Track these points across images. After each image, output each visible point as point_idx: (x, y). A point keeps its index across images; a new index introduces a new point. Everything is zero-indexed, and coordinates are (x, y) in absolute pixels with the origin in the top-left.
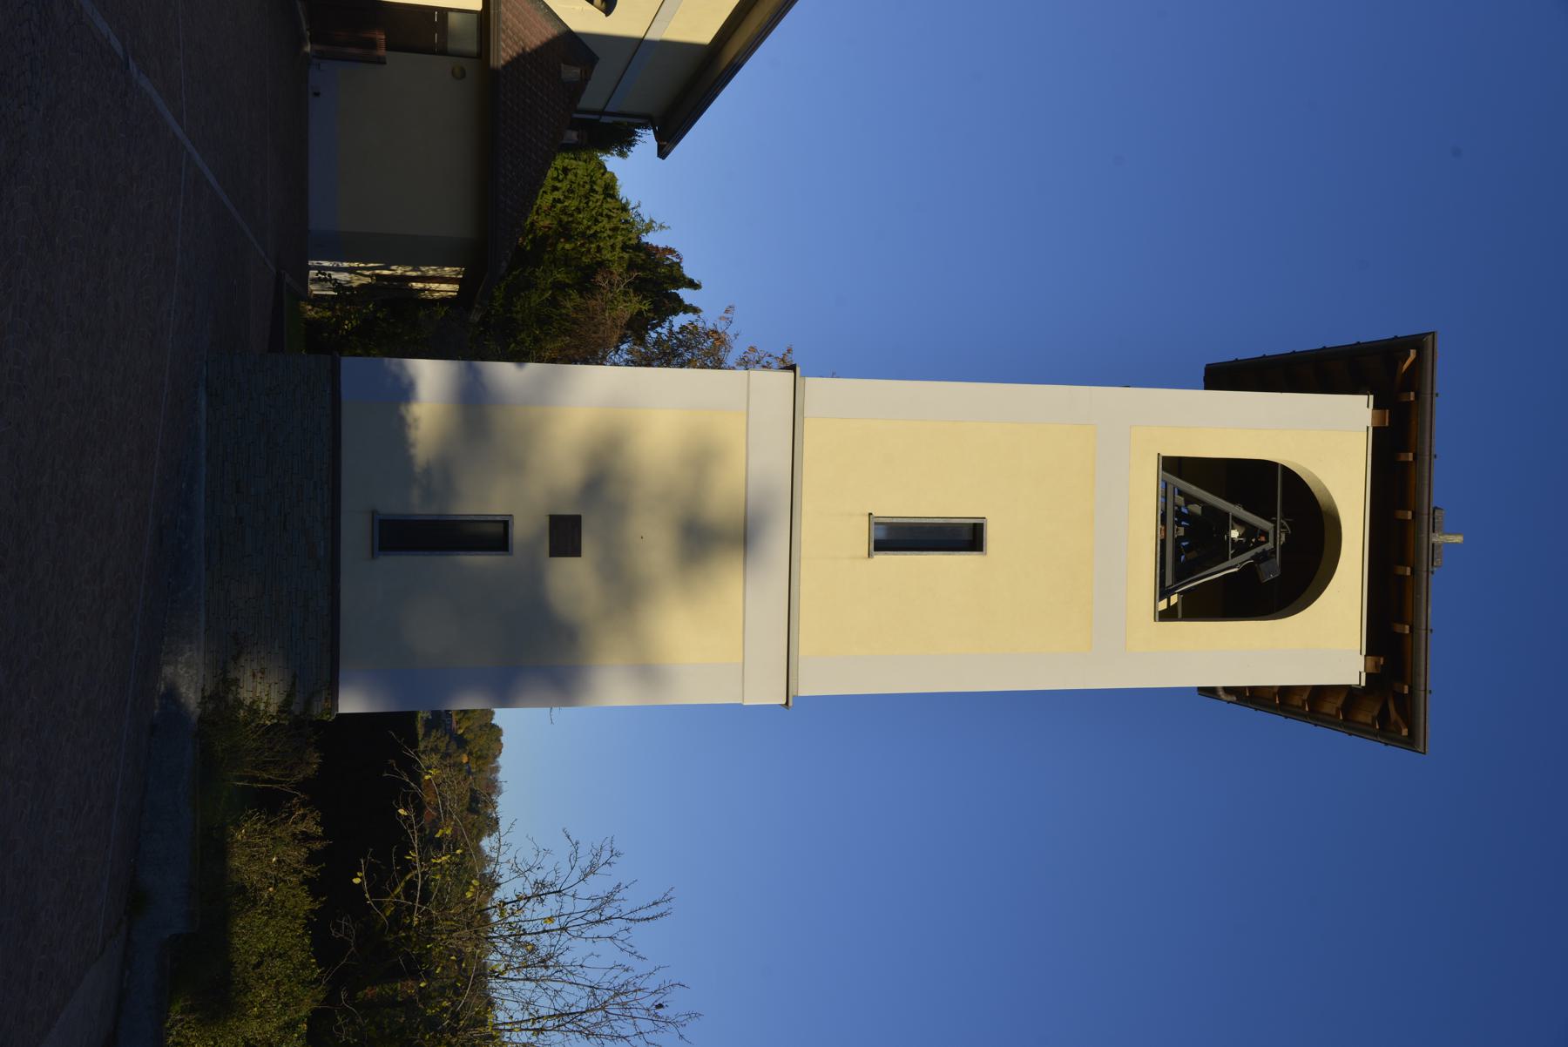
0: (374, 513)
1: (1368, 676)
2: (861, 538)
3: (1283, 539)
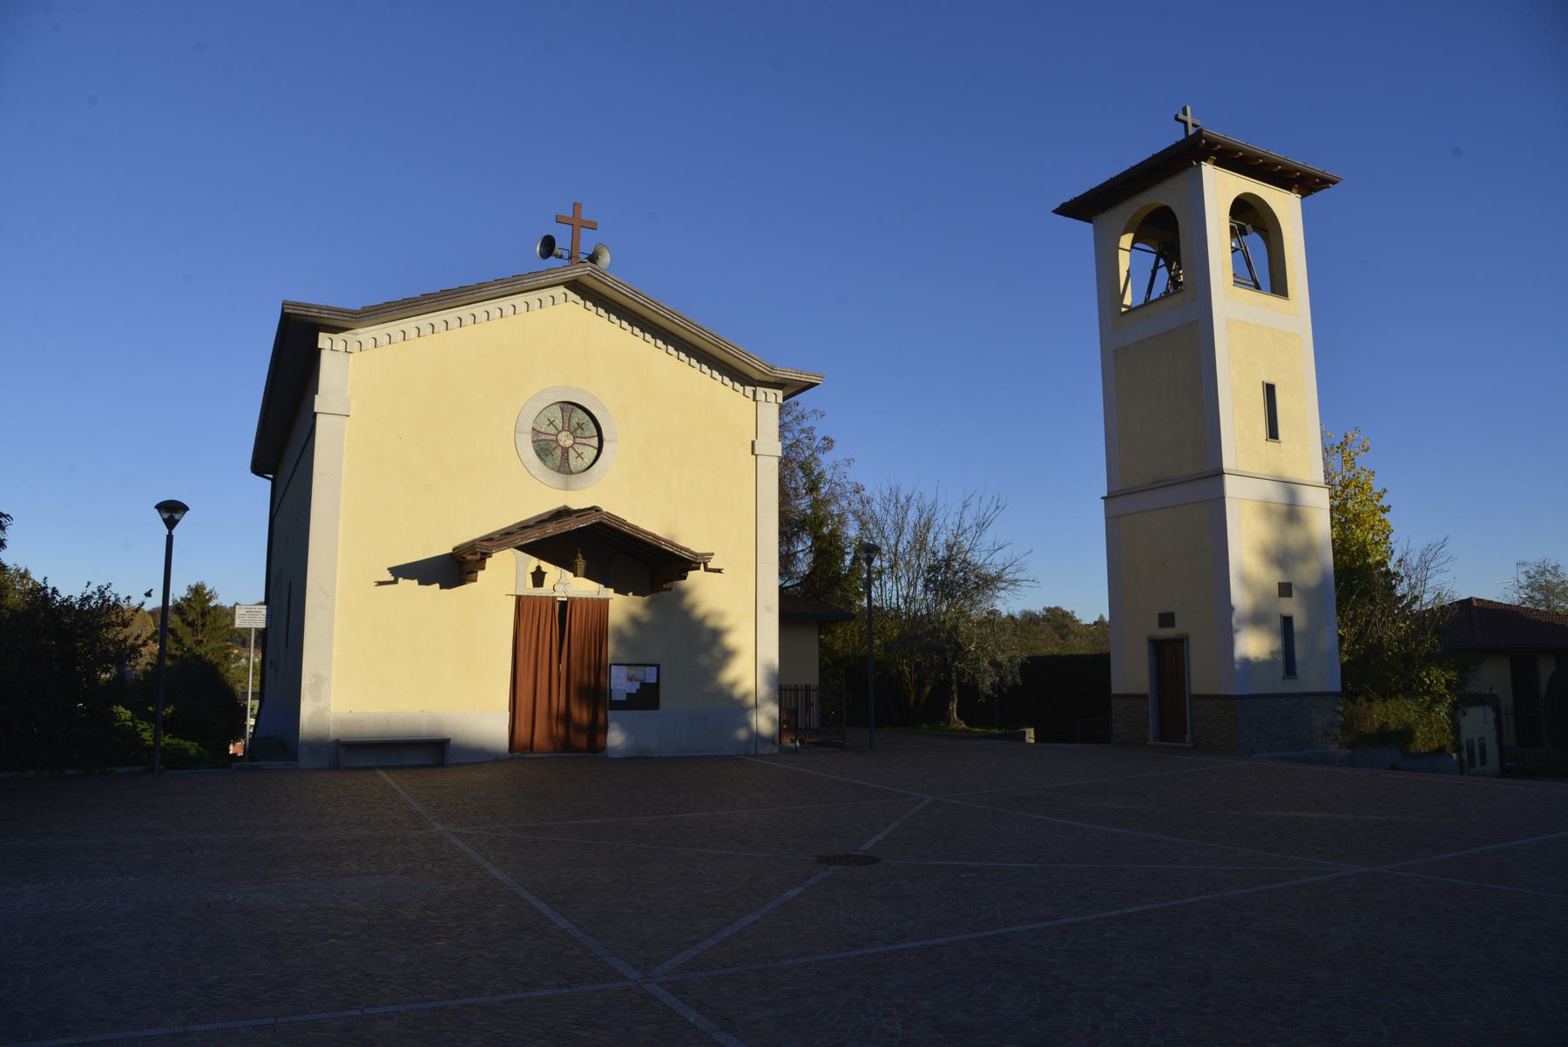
0: (1284, 678)
1: (1298, 193)
2: (1272, 444)
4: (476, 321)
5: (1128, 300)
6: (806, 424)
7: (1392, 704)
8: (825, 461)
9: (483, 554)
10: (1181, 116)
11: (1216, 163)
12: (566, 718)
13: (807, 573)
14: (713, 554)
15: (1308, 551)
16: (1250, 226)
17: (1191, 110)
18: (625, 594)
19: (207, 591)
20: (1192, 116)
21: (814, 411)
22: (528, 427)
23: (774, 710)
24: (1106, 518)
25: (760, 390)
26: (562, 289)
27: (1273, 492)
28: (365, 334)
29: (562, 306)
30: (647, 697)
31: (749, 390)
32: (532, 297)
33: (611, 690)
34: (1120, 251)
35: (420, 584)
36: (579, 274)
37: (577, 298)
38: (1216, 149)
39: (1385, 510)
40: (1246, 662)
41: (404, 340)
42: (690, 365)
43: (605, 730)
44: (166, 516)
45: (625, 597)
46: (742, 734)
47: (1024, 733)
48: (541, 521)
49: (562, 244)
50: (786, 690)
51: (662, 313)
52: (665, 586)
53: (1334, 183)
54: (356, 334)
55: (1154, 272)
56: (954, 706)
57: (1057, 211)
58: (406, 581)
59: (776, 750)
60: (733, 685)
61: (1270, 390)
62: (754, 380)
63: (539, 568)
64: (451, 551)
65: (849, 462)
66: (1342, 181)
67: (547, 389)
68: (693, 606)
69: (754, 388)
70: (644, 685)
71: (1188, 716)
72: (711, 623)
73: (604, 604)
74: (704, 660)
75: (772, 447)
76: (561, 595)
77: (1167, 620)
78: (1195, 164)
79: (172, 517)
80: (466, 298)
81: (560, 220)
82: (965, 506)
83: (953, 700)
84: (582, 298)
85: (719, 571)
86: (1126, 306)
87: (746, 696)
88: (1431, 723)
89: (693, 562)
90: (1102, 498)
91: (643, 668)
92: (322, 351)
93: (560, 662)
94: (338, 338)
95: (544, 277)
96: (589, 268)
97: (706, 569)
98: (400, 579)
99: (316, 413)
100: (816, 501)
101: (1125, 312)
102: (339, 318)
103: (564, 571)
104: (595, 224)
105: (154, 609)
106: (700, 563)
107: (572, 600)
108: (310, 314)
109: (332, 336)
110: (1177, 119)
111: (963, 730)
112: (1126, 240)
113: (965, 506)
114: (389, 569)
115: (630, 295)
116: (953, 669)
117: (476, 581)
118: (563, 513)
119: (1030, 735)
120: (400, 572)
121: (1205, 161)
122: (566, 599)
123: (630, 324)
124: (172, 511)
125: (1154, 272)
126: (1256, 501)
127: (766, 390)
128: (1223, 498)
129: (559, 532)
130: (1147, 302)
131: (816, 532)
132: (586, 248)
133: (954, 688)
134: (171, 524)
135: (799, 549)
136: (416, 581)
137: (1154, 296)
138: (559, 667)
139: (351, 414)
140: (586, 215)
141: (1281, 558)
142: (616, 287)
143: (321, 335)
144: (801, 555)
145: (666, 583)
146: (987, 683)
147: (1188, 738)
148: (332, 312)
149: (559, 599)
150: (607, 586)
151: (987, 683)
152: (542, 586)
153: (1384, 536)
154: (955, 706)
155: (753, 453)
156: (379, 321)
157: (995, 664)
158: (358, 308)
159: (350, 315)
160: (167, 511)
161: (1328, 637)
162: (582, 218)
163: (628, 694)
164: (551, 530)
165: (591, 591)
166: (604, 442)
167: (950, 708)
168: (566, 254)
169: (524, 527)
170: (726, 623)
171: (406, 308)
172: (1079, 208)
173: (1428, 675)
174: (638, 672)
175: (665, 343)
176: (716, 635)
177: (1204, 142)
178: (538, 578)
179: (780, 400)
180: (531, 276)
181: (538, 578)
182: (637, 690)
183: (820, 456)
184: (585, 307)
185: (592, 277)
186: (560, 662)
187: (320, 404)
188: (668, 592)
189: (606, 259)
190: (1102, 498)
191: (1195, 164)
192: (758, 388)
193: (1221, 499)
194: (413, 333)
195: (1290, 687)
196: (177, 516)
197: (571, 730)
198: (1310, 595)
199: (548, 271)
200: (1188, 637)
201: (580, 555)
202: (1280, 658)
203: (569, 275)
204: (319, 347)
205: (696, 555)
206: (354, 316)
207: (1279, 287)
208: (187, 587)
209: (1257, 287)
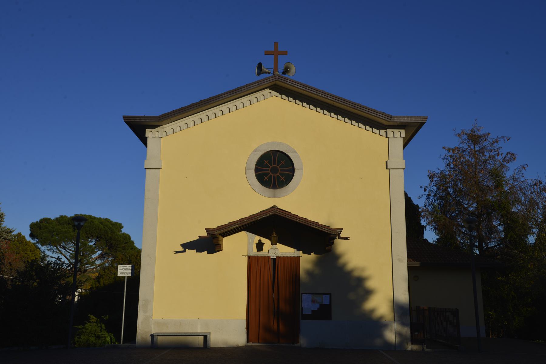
21: (503, 137)
25: (390, 132)
26: (268, 91)
28: (168, 127)
31: (383, 132)
37: (277, 94)
40: (117, 268)
54: (163, 128)
62: (385, 125)
63: (260, 241)
65: (523, 167)
69: (386, 130)
70: (322, 306)
73: (297, 259)
76: (273, 255)
81: (267, 53)
85: (347, 238)
89: (332, 234)
96: (278, 77)
98: (187, 250)
107: (279, 258)
109: (152, 130)
114: (181, 245)
120: (187, 246)
122: (275, 257)
132: (281, 66)
136: (195, 251)
140: (280, 49)
149: (271, 257)
152: (262, 250)
155: (387, 168)
178: (260, 246)
181: (260, 246)
189: (293, 70)
201: (274, 233)
204: (146, 136)
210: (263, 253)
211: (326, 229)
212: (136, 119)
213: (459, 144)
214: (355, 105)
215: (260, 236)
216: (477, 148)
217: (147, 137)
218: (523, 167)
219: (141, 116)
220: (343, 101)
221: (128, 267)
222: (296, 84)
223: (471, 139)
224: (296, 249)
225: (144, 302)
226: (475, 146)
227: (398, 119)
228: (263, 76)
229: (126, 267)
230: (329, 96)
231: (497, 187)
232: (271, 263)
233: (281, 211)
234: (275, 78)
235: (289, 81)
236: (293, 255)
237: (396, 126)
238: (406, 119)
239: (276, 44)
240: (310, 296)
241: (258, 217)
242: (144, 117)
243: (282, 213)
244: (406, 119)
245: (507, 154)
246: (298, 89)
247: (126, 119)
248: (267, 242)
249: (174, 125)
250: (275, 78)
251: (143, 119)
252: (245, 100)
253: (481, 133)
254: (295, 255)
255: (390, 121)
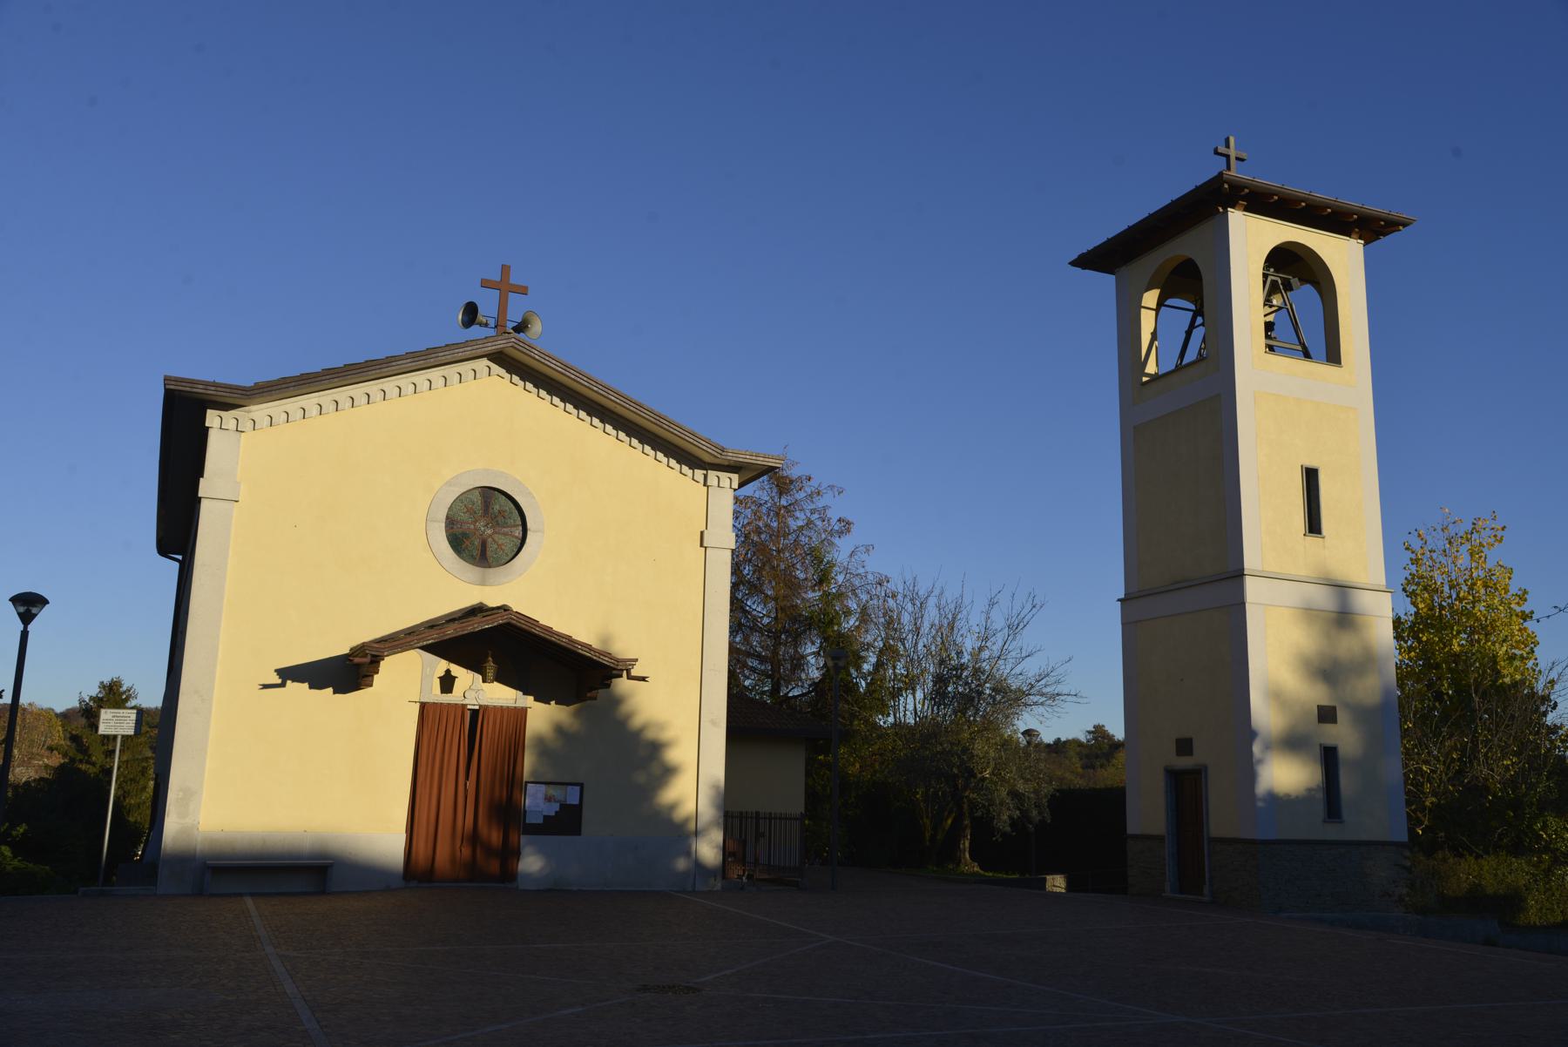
0: (1325, 821)
2: (1312, 540)
3: (1272, 270)
4: (478, 376)
5: (1151, 368)
6: (820, 503)
7: (1489, 863)
8: (841, 552)
9: (373, 656)
10: (1222, 149)
11: (1247, 209)
12: (474, 838)
13: (817, 681)
14: (637, 660)
15: (1367, 661)
16: (1297, 279)
17: (1235, 141)
18: (548, 702)
19: (124, 688)
20: (1236, 148)
21: (831, 487)
22: (442, 515)
23: (717, 836)
24: (1123, 624)
25: (712, 474)
26: (485, 362)
27: (1322, 598)
28: (260, 411)
29: (484, 380)
30: (566, 821)
31: (699, 474)
32: (451, 371)
33: (525, 811)
34: (1143, 310)
35: (311, 688)
36: (501, 346)
37: (502, 372)
38: (1243, 193)
39: (1526, 617)
40: (1273, 798)
41: (304, 418)
42: (630, 445)
43: (517, 854)
44: (22, 609)
45: (547, 705)
46: (681, 864)
47: (1045, 880)
48: (452, 619)
49: (487, 310)
50: (775, 818)
51: (595, 389)
52: (589, 695)
53: (1405, 225)
54: (249, 412)
55: (1189, 334)
56: (966, 844)
57: (1074, 263)
58: (296, 684)
59: (718, 885)
60: (673, 807)
61: (1311, 476)
62: (705, 462)
63: (448, 671)
64: (348, 652)
65: (868, 549)
66: (1415, 223)
67: (465, 472)
68: (629, 716)
69: (705, 472)
70: (565, 807)
71: (1206, 863)
72: (650, 735)
73: (521, 714)
74: (641, 778)
75: (724, 538)
76: (472, 702)
77: (1184, 747)
78: (1221, 210)
79: (28, 611)
80: (373, 374)
81: (486, 284)
82: (992, 604)
83: (965, 837)
84: (508, 371)
85: (643, 679)
86: (1147, 375)
87: (687, 820)
88: (1550, 889)
89: (615, 669)
90: (1119, 600)
91: (563, 787)
92: (210, 430)
93: (467, 777)
94: (229, 416)
95: (461, 350)
96: (513, 340)
97: (630, 677)
98: (289, 682)
99: (200, 498)
100: (826, 594)
101: (1147, 382)
102: (228, 394)
103: (476, 674)
104: (526, 288)
105: (68, 710)
106: (622, 670)
107: (484, 708)
108: (195, 390)
109: (223, 413)
110: (1216, 152)
111: (975, 874)
112: (1151, 298)
113: (992, 604)
114: (276, 671)
115: (560, 369)
116: (965, 800)
117: (371, 686)
118: (478, 610)
119: (1057, 883)
120: (289, 674)
121: (1233, 207)
122: (477, 707)
123: (562, 400)
124: (28, 605)
125: (1189, 334)
126: (1299, 608)
127: (719, 474)
128: (1243, 604)
129: (461, 633)
130: (1179, 368)
131: (824, 632)
132: (514, 317)
133: (966, 822)
134: (27, 618)
135: (809, 651)
136: (306, 685)
137: (1188, 359)
138: (466, 784)
139: (240, 499)
140: (514, 279)
141: (1328, 671)
142: (543, 361)
143: (210, 413)
144: (811, 659)
145: (589, 692)
146: (1004, 818)
147: (1206, 890)
148: (219, 389)
149: (469, 707)
150: (526, 693)
151: (1004, 818)
152: (451, 692)
153: (1528, 649)
154: (967, 844)
155: (702, 545)
156: (275, 397)
157: (1014, 794)
158: (249, 383)
159: (240, 392)
160: (23, 605)
161: (1392, 770)
162: (512, 281)
163: (545, 817)
164: (451, 631)
165: (507, 699)
166: (529, 532)
167: (961, 846)
168: (492, 323)
169: (432, 625)
170: (666, 735)
171: (263, 392)
172: (1096, 260)
173: (1544, 828)
174: (552, 791)
175: (602, 421)
176: (655, 749)
177: (1226, 186)
178: (447, 683)
179: (735, 485)
180: (447, 348)
181: (447, 683)
182: (556, 812)
183: (836, 541)
184: (511, 382)
185: (515, 348)
186: (467, 777)
187: (205, 487)
188: (594, 702)
189: (536, 328)
190: (1119, 600)
191: (1221, 210)
192: (709, 471)
193: (1240, 605)
194: (315, 410)
195: (1332, 833)
196: (34, 610)
197: (478, 851)
198: (1365, 716)
199: (466, 344)
200: (1206, 768)
201: (490, 659)
202: (1320, 795)
203: (490, 348)
204: (207, 425)
205: (618, 661)
206: (244, 392)
207: (1333, 356)
208: (98, 684)
209: (1307, 355)
210: (454, 699)
211: (606, 659)
212: (195, 386)
213: (755, 492)
214: (658, 418)
215: (451, 660)
216: (784, 502)
217: (208, 428)
218: (868, 549)
219: (209, 382)
220: (638, 407)
221: (125, 715)
222: (550, 360)
223: (777, 486)
224: (520, 690)
225: (181, 793)
226: (780, 498)
227: (734, 455)
228: (475, 332)
229: (121, 715)
230: (612, 393)
231: (821, 582)
232: (468, 714)
233: (520, 617)
234: (508, 341)
235: (536, 352)
236: (514, 705)
237: (724, 466)
238: (748, 457)
239: (505, 269)
240: (543, 787)
241: (476, 626)
242: (215, 385)
243: (523, 622)
244: (748, 457)
245: (839, 520)
246: (552, 370)
247: (169, 382)
248: (464, 677)
249: (276, 408)
250: (508, 341)
251: (213, 388)
252: (436, 374)
253: (794, 473)
254: (517, 705)
255: (719, 456)
